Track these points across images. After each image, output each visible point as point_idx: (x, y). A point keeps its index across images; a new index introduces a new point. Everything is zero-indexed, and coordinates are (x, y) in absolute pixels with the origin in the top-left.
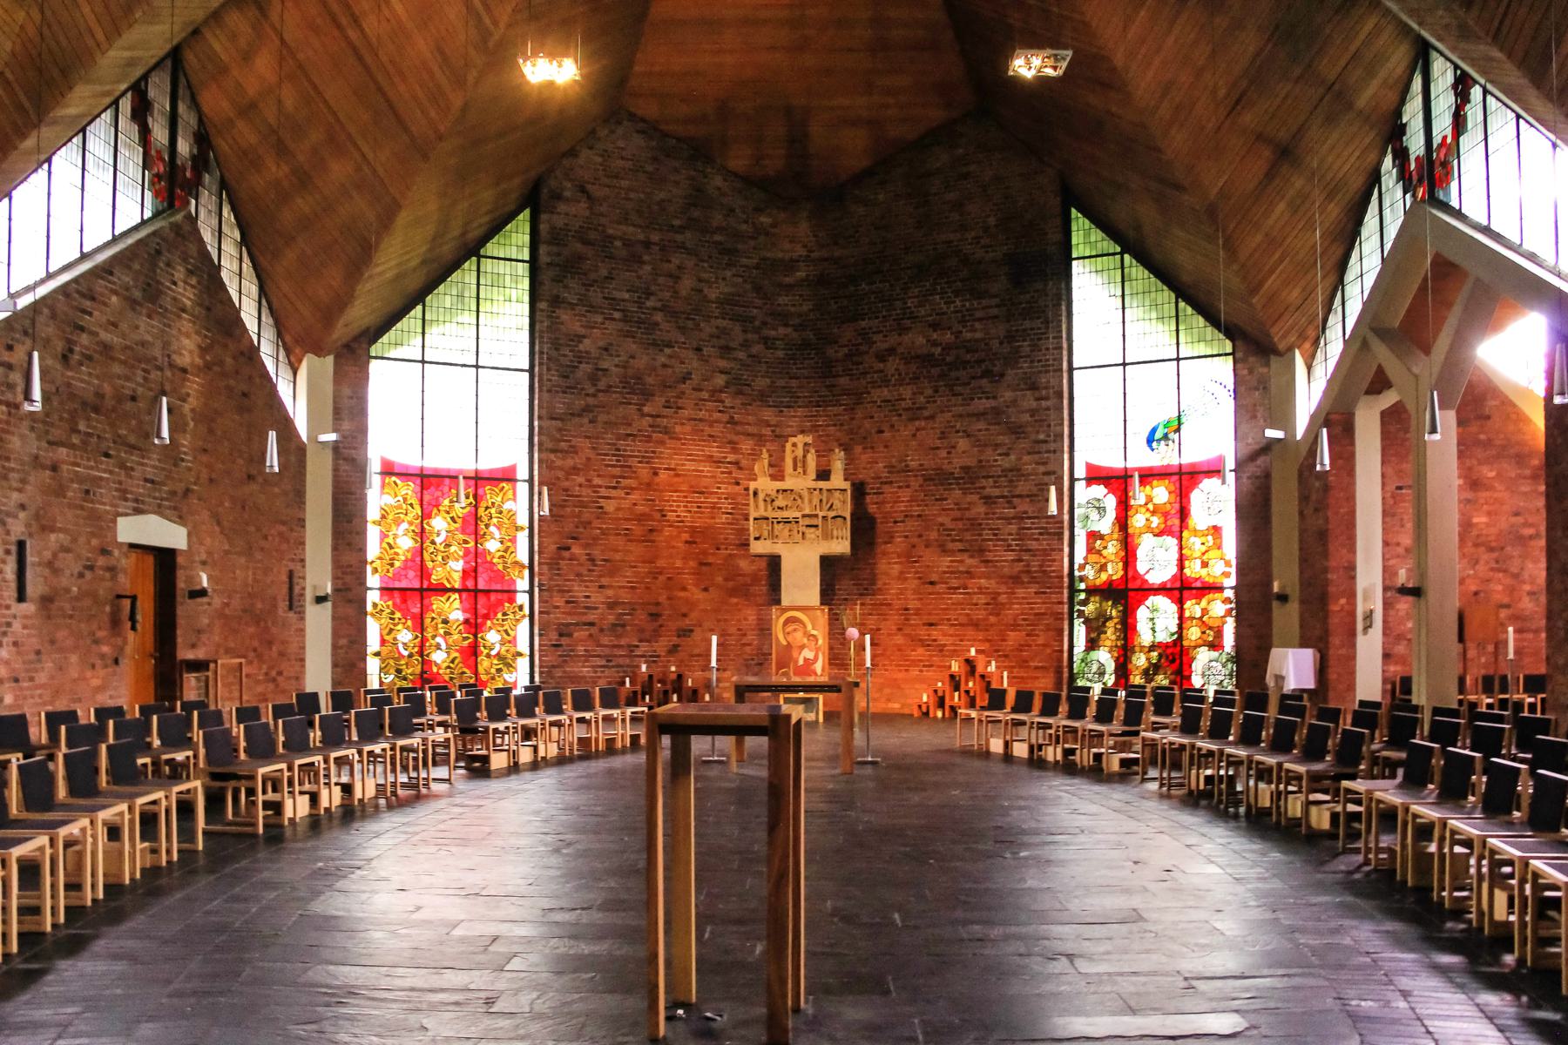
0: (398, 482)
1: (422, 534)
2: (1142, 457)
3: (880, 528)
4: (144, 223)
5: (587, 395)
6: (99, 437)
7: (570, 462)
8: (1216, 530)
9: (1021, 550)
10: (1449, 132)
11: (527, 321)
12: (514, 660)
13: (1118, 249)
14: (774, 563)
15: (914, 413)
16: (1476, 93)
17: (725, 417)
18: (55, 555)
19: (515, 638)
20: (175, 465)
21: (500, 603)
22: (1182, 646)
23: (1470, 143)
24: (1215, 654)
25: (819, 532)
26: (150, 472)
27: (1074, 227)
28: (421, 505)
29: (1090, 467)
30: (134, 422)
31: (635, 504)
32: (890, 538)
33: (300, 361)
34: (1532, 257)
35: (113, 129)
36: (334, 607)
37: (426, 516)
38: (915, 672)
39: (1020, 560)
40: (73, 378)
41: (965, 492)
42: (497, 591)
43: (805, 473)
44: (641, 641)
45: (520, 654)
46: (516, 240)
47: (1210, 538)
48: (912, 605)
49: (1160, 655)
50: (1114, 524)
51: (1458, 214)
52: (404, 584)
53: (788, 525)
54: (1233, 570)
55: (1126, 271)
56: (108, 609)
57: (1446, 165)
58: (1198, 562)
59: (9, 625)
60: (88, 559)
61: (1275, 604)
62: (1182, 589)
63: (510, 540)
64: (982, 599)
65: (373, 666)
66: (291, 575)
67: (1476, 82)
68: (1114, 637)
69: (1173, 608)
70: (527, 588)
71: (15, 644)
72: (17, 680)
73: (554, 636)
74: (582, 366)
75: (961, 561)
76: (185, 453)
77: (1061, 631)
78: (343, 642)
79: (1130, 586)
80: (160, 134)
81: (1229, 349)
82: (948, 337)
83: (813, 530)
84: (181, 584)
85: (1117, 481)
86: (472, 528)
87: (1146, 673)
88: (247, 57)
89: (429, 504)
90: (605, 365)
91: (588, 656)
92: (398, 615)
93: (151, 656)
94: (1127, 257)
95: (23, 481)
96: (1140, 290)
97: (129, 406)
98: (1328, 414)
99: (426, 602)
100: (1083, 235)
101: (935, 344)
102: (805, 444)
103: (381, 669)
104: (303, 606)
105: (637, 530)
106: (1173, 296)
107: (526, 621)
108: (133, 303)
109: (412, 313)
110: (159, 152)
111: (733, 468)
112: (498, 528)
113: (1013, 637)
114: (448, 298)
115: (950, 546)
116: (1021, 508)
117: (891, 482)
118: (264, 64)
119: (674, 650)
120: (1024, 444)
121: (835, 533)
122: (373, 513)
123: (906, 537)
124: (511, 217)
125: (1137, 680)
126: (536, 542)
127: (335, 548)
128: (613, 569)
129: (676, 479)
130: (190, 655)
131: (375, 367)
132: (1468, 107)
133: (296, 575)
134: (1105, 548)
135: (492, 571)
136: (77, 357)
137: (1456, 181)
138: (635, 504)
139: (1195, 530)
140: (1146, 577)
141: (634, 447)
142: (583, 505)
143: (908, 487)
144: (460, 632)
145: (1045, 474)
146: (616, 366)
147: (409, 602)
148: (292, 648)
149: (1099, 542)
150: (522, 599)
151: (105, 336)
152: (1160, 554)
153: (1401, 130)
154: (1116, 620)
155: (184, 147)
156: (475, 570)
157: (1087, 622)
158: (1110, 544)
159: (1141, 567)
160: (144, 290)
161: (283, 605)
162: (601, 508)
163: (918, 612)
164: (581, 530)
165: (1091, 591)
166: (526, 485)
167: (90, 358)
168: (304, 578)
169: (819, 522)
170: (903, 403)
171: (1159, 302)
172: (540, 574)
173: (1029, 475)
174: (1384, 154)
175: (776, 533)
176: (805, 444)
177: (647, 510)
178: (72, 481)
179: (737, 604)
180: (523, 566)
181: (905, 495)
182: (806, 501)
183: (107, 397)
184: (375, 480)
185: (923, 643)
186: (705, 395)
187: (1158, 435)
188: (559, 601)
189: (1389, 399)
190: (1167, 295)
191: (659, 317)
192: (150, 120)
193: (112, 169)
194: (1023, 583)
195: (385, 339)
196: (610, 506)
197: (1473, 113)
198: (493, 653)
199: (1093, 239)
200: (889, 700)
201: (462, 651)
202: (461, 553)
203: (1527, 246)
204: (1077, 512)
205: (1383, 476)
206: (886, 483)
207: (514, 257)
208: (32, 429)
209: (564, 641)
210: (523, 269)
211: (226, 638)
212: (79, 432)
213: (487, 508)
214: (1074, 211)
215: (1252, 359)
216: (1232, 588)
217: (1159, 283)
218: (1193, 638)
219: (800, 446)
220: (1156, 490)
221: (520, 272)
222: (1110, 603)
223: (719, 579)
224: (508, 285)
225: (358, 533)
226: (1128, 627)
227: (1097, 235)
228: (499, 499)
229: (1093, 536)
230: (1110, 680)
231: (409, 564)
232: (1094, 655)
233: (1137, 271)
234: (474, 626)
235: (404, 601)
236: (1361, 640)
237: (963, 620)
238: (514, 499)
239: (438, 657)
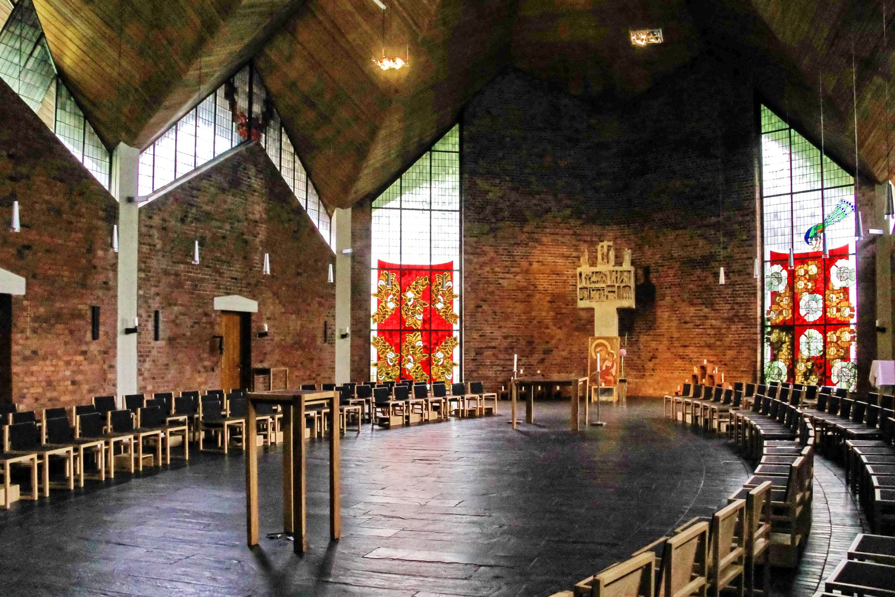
1: (401, 301)
2: (802, 248)
3: (659, 292)
4: (232, 149)
7: (482, 259)
8: (845, 290)
9: (734, 303)
11: (458, 184)
12: (452, 368)
15: (675, 227)
17: (571, 232)
18: (177, 317)
20: (251, 269)
21: (444, 337)
22: (826, 359)
24: (845, 364)
25: (616, 295)
26: (235, 275)
27: (763, 115)
28: (400, 285)
29: (773, 254)
32: (663, 297)
33: (333, 212)
35: (214, 105)
36: (352, 340)
37: (403, 290)
38: (676, 374)
41: (703, 270)
42: (442, 330)
45: (454, 364)
46: (452, 141)
47: (841, 294)
48: (676, 335)
49: (813, 365)
50: (786, 287)
52: (390, 328)
53: (598, 292)
54: (855, 313)
55: (792, 139)
58: (835, 309)
59: (150, 352)
62: (825, 325)
64: (712, 332)
65: (374, 371)
68: (787, 353)
69: (820, 336)
70: (458, 328)
71: (154, 361)
72: (154, 378)
73: (473, 354)
77: (756, 351)
78: (356, 358)
79: (796, 323)
80: (242, 103)
81: (852, 182)
82: (693, 182)
83: (612, 294)
84: (254, 330)
86: (428, 297)
87: (805, 375)
88: (289, 59)
89: (405, 284)
91: (493, 365)
92: (387, 344)
93: (237, 366)
94: (792, 130)
95: (159, 282)
96: (800, 150)
99: (402, 337)
100: (769, 119)
101: (687, 186)
102: (609, 246)
103: (378, 373)
105: (521, 296)
106: (819, 152)
107: (458, 347)
108: (223, 190)
111: (576, 260)
112: (442, 297)
113: (730, 354)
114: (414, 174)
115: (695, 301)
118: (299, 63)
119: (542, 361)
120: (735, 242)
121: (625, 295)
122: (374, 290)
124: (449, 128)
125: (799, 379)
127: (352, 309)
128: (507, 317)
129: (543, 267)
130: (259, 366)
131: (375, 213)
133: (328, 323)
134: (782, 301)
136: (189, 219)
139: (833, 290)
140: (805, 318)
141: (519, 251)
142: (488, 283)
144: (421, 353)
147: (394, 337)
148: (327, 362)
149: (778, 298)
150: (456, 334)
151: (208, 208)
154: (788, 343)
155: (257, 109)
156: (430, 319)
157: (772, 344)
158: (784, 300)
159: (802, 312)
161: (319, 341)
162: (500, 284)
163: (678, 339)
164: (488, 296)
165: (773, 327)
166: (458, 273)
169: (616, 289)
171: (811, 156)
172: (465, 321)
173: (737, 259)
175: (592, 296)
176: (609, 246)
177: (525, 284)
178: (187, 280)
179: (578, 336)
180: (456, 316)
181: (671, 272)
182: (609, 277)
183: (208, 239)
184: (374, 274)
185: (682, 358)
186: (559, 220)
188: (475, 335)
190: (816, 152)
191: (533, 179)
193: (213, 124)
194: (734, 322)
195: (380, 198)
196: (505, 283)
198: (440, 364)
199: (773, 121)
200: (662, 389)
201: (422, 363)
204: (767, 280)
207: (450, 150)
208: (163, 256)
209: (478, 358)
210: (456, 157)
211: (283, 358)
213: (436, 286)
214: (762, 106)
215: (864, 187)
217: (811, 145)
218: (832, 354)
220: (810, 267)
221: (454, 158)
222: (784, 333)
223: (568, 322)
224: (447, 165)
225: (365, 301)
226: (795, 348)
227: (775, 118)
229: (774, 294)
230: (784, 379)
231: (394, 317)
232: (775, 364)
233: (798, 138)
234: (429, 349)
235: (391, 336)
237: (702, 344)
238: (452, 281)
239: (409, 366)
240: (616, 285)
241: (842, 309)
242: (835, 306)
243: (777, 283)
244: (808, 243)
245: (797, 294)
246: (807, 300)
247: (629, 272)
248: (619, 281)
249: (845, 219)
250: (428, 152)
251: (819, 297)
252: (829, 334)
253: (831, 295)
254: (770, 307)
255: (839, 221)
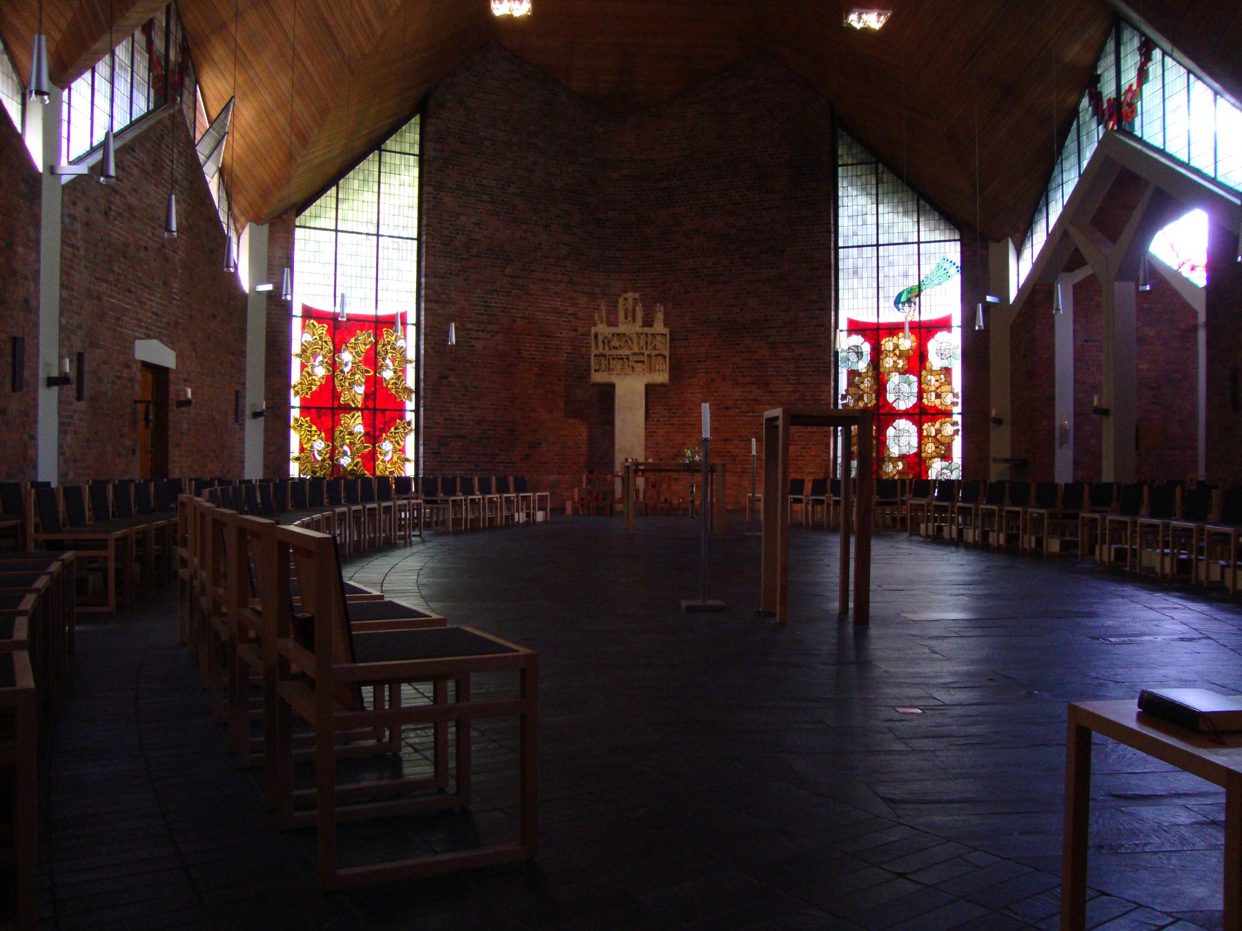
0: (316, 324)
1: (334, 366)
2: (890, 315)
5: (462, 259)
6: (125, 277)
8: (947, 371)
9: (799, 384)
10: (1134, 82)
12: (403, 465)
13: (874, 160)
14: (608, 391)
16: (1157, 54)
19: (404, 446)
22: (921, 457)
23: (1151, 90)
24: (945, 464)
28: (333, 341)
30: (146, 267)
31: (498, 344)
33: (243, 228)
34: (1197, 172)
36: (266, 422)
37: (337, 350)
39: (797, 391)
40: (111, 230)
43: (634, 321)
44: (501, 450)
45: (408, 460)
46: (410, 137)
47: (942, 376)
50: (868, 365)
51: (1140, 140)
54: (960, 400)
55: (880, 175)
56: (129, 410)
57: (1132, 106)
58: (933, 394)
60: (118, 371)
61: (992, 425)
62: (921, 414)
63: (401, 371)
66: (237, 392)
67: (1156, 46)
69: (914, 429)
74: (459, 237)
75: (750, 392)
76: (176, 293)
79: (881, 411)
80: (159, 45)
83: (640, 364)
84: (172, 396)
85: (874, 333)
90: (477, 236)
92: (314, 428)
94: (880, 166)
97: (142, 254)
98: (1035, 285)
102: (634, 299)
104: (244, 420)
109: (329, 192)
110: (158, 58)
114: (356, 182)
116: (797, 352)
117: (696, 331)
121: (657, 367)
122: (296, 348)
123: (706, 373)
124: (406, 120)
126: (422, 373)
131: (299, 233)
132: (1150, 64)
134: (862, 383)
135: (388, 395)
137: (1140, 117)
138: (498, 344)
139: (932, 370)
143: (709, 334)
145: (818, 326)
146: (485, 237)
151: (132, 200)
152: (905, 388)
153: (1097, 79)
156: (374, 393)
159: (890, 398)
160: (153, 165)
161: (231, 418)
162: (472, 346)
166: (414, 327)
167: (121, 215)
168: (244, 398)
170: (705, 270)
172: (425, 398)
174: (1082, 97)
175: (612, 366)
176: (634, 299)
182: (635, 342)
184: (296, 324)
187: (903, 299)
189: (1080, 275)
192: (153, 33)
195: (307, 212)
196: (479, 345)
197: (1154, 69)
201: (363, 457)
202: (363, 380)
203: (1193, 164)
205: (1075, 331)
206: (691, 331)
207: (407, 151)
212: (113, 272)
213: (384, 345)
216: (959, 414)
218: (930, 451)
219: (630, 301)
221: (412, 163)
228: (393, 338)
229: (852, 374)
234: (373, 436)
235: (319, 417)
236: (1059, 453)
238: (405, 339)
240: (646, 353)
241: (943, 395)
242: (934, 391)
243: (856, 360)
244: (899, 310)
245: (883, 374)
246: (897, 382)
247: (665, 335)
248: (650, 347)
249: (948, 282)
250: (377, 152)
251: (913, 378)
252: (925, 426)
253: (929, 377)
254: (846, 391)
255: (940, 284)
